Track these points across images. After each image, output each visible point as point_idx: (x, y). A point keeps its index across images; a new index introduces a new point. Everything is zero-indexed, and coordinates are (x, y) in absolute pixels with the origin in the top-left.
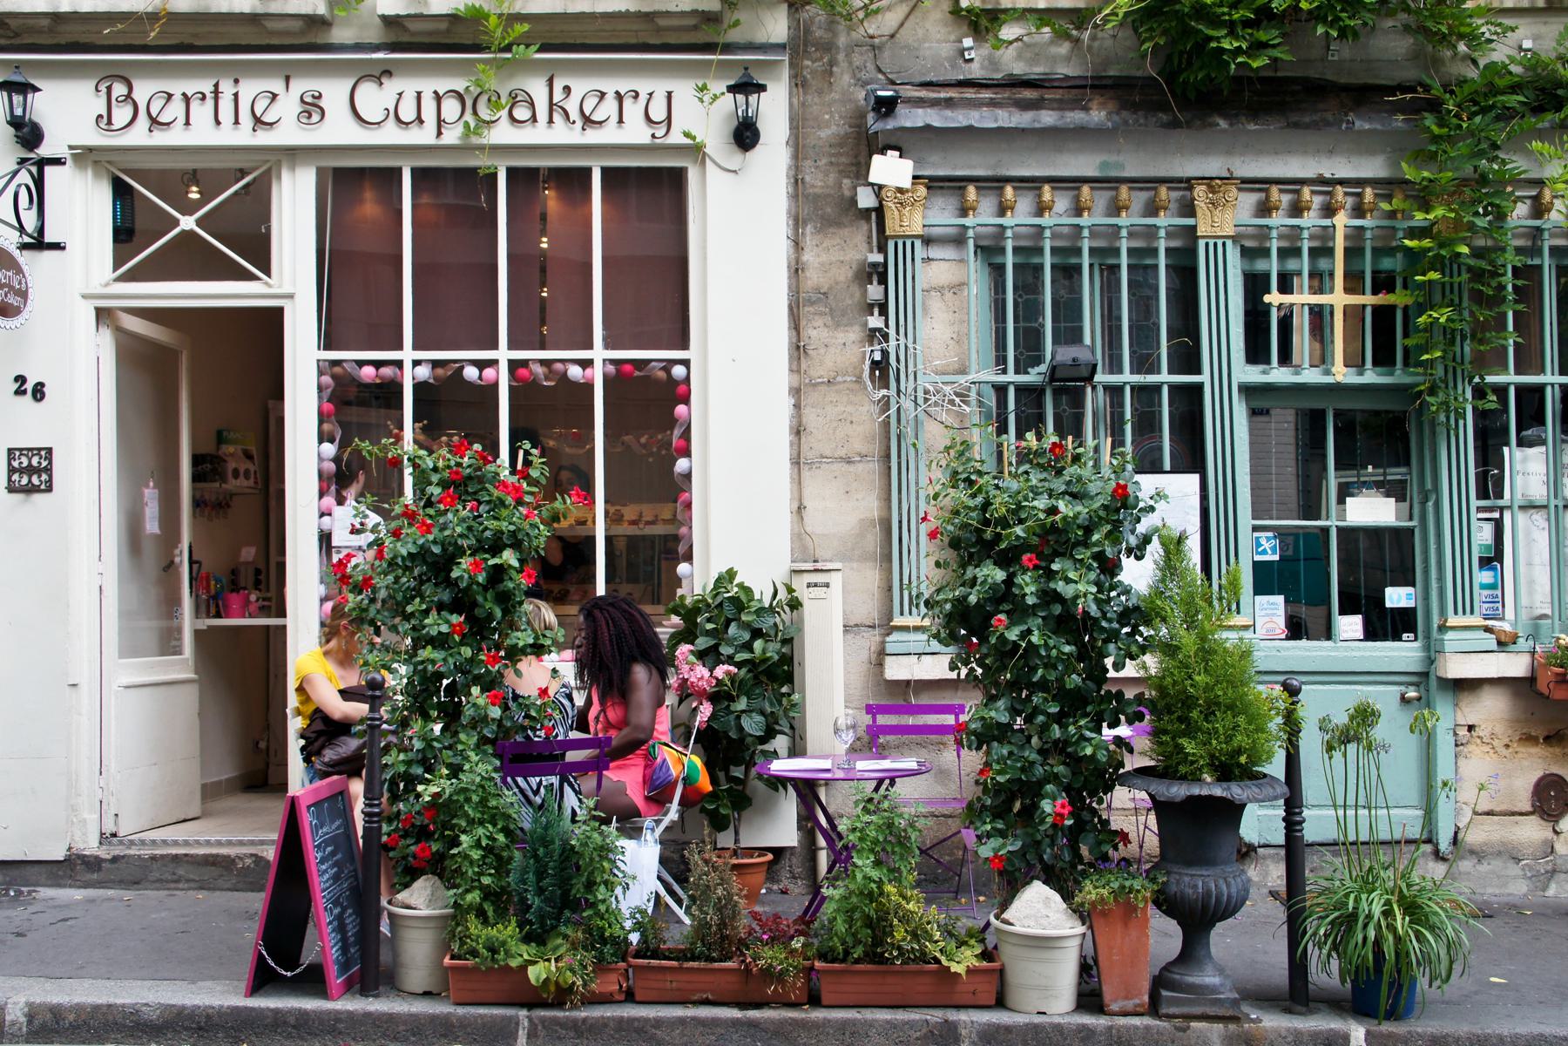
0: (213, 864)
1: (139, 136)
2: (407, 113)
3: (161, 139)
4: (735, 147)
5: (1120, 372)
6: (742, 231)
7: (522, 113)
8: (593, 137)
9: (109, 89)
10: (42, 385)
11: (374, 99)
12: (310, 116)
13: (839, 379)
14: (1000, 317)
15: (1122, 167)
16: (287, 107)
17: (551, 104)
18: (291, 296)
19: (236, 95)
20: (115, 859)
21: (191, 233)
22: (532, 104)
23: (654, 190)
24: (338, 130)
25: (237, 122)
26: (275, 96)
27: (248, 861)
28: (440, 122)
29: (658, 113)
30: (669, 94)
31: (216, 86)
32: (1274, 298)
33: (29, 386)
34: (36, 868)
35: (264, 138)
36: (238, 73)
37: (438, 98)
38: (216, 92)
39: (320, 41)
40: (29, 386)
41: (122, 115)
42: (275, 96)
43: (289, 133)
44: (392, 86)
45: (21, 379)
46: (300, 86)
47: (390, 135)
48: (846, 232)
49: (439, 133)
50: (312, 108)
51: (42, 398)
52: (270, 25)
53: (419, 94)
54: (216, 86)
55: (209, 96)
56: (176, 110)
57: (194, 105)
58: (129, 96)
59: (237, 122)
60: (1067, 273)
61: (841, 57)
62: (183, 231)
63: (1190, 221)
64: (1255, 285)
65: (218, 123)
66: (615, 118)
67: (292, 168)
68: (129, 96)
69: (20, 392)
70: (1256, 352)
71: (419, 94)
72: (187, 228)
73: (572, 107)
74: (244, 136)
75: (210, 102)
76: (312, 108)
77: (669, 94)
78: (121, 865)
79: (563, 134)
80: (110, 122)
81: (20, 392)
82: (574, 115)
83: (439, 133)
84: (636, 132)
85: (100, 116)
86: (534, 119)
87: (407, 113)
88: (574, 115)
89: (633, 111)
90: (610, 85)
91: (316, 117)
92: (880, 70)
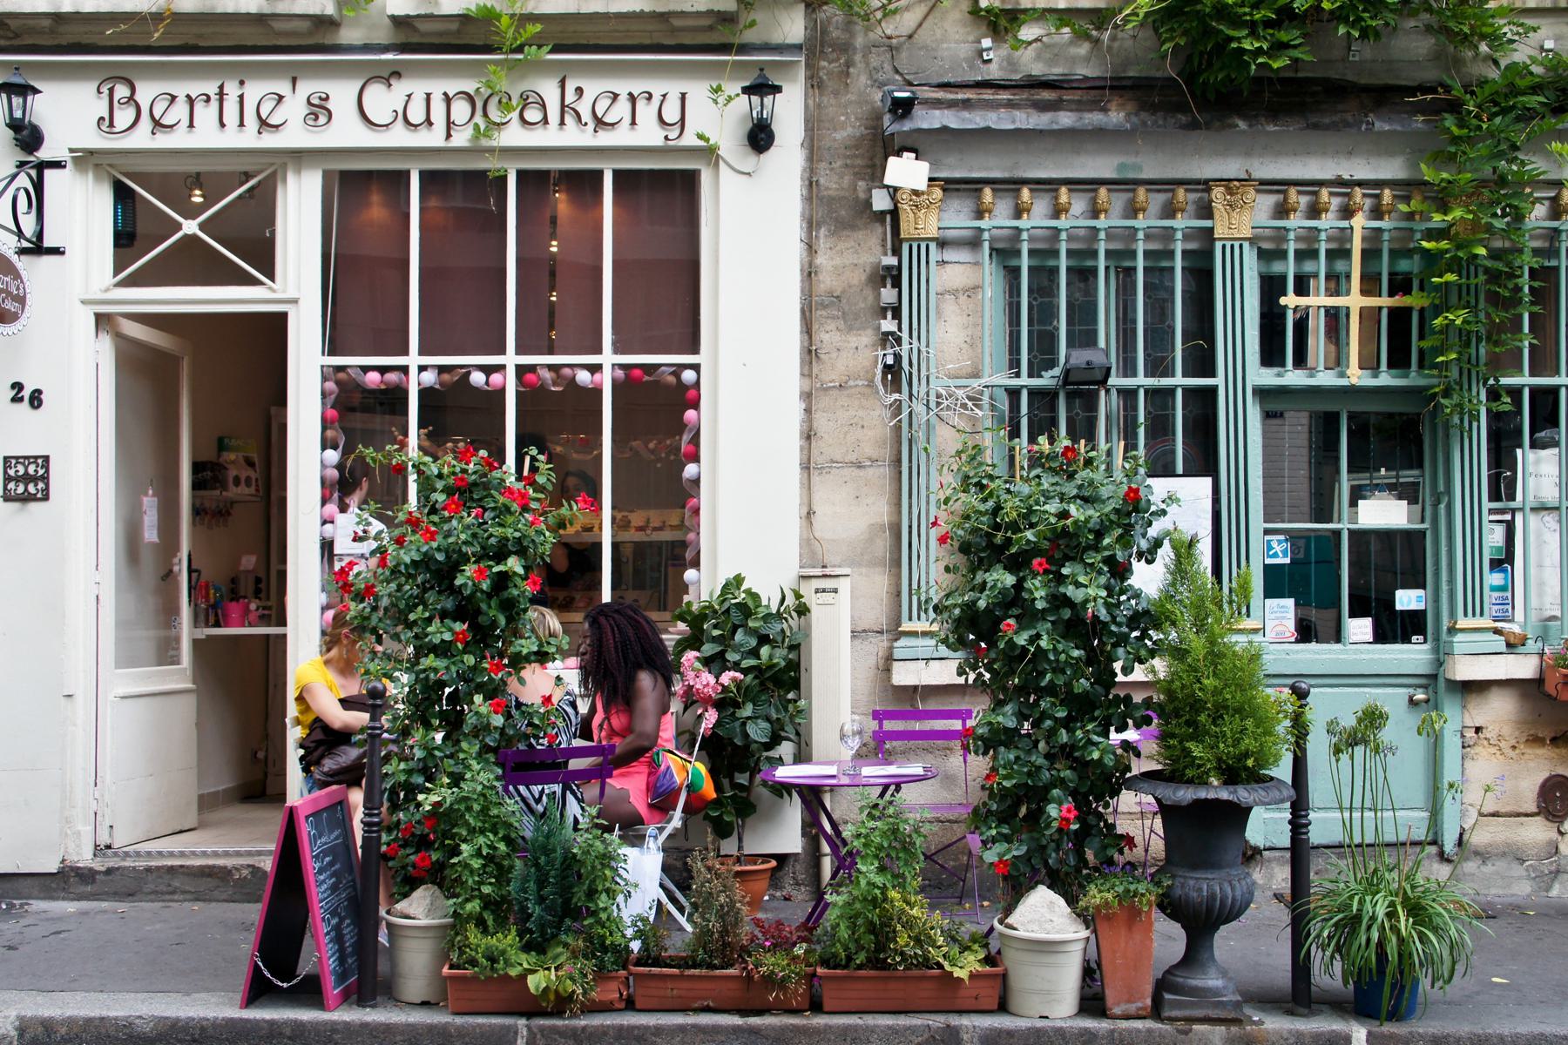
0: (210, 875)
1: (143, 138)
2: (416, 115)
3: (164, 141)
4: (749, 149)
5: (1134, 375)
6: (755, 234)
7: (533, 115)
8: (605, 139)
9: (111, 90)
10: (39, 392)
11: (382, 101)
12: (317, 118)
13: (851, 383)
14: (1014, 320)
15: (1140, 169)
16: (294, 108)
17: (563, 106)
18: (295, 301)
19: (241, 97)
20: (109, 871)
21: (194, 237)
22: (544, 106)
23: (666, 194)
24: (345, 132)
25: (242, 124)
26: (281, 98)
27: (245, 872)
28: (450, 124)
29: (671, 115)
30: (683, 96)
31: (221, 87)
32: (1290, 300)
33: (26, 393)
34: (29, 881)
35: (270, 141)
36: (243, 74)
37: (448, 100)
38: (221, 94)
39: (328, 41)
40: (26, 393)
41: (124, 117)
42: (281, 98)
43: (295, 135)
44: (401, 88)
45: (18, 386)
46: (307, 88)
47: (399, 137)
48: (860, 234)
49: (449, 136)
50: (319, 110)
51: (40, 405)
52: (277, 25)
53: (428, 95)
54: (221, 87)
55: (214, 98)
56: (179, 112)
57: (199, 107)
58: (131, 98)
59: (242, 124)
60: (1083, 275)
61: (858, 57)
62: (186, 236)
63: (1207, 223)
64: (1272, 287)
65: (222, 125)
66: (628, 119)
67: (298, 171)
68: (131, 98)
69: (17, 399)
70: (1271, 355)
71: (428, 95)
72: (190, 232)
73: (584, 109)
74: (249, 139)
75: (214, 104)
76: (319, 110)
77: (683, 96)
78: (116, 877)
79: (573, 136)
80: (111, 125)
81: (17, 399)
82: (586, 116)
83: (449, 136)
84: (649, 134)
85: (102, 119)
86: (545, 121)
87: (416, 115)
88: (586, 116)
89: (646, 112)
90: (623, 87)
91: (322, 120)
92: (897, 72)
